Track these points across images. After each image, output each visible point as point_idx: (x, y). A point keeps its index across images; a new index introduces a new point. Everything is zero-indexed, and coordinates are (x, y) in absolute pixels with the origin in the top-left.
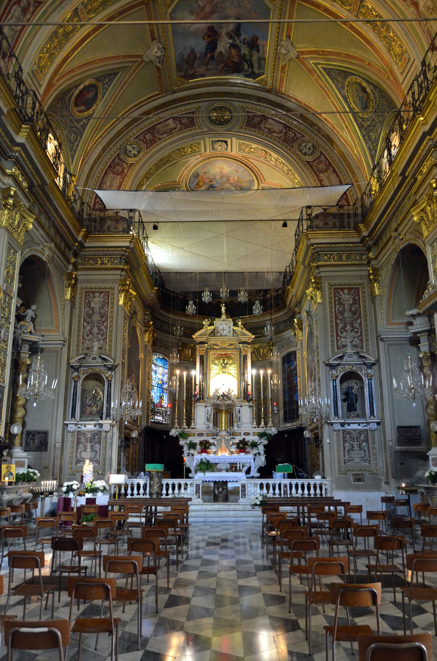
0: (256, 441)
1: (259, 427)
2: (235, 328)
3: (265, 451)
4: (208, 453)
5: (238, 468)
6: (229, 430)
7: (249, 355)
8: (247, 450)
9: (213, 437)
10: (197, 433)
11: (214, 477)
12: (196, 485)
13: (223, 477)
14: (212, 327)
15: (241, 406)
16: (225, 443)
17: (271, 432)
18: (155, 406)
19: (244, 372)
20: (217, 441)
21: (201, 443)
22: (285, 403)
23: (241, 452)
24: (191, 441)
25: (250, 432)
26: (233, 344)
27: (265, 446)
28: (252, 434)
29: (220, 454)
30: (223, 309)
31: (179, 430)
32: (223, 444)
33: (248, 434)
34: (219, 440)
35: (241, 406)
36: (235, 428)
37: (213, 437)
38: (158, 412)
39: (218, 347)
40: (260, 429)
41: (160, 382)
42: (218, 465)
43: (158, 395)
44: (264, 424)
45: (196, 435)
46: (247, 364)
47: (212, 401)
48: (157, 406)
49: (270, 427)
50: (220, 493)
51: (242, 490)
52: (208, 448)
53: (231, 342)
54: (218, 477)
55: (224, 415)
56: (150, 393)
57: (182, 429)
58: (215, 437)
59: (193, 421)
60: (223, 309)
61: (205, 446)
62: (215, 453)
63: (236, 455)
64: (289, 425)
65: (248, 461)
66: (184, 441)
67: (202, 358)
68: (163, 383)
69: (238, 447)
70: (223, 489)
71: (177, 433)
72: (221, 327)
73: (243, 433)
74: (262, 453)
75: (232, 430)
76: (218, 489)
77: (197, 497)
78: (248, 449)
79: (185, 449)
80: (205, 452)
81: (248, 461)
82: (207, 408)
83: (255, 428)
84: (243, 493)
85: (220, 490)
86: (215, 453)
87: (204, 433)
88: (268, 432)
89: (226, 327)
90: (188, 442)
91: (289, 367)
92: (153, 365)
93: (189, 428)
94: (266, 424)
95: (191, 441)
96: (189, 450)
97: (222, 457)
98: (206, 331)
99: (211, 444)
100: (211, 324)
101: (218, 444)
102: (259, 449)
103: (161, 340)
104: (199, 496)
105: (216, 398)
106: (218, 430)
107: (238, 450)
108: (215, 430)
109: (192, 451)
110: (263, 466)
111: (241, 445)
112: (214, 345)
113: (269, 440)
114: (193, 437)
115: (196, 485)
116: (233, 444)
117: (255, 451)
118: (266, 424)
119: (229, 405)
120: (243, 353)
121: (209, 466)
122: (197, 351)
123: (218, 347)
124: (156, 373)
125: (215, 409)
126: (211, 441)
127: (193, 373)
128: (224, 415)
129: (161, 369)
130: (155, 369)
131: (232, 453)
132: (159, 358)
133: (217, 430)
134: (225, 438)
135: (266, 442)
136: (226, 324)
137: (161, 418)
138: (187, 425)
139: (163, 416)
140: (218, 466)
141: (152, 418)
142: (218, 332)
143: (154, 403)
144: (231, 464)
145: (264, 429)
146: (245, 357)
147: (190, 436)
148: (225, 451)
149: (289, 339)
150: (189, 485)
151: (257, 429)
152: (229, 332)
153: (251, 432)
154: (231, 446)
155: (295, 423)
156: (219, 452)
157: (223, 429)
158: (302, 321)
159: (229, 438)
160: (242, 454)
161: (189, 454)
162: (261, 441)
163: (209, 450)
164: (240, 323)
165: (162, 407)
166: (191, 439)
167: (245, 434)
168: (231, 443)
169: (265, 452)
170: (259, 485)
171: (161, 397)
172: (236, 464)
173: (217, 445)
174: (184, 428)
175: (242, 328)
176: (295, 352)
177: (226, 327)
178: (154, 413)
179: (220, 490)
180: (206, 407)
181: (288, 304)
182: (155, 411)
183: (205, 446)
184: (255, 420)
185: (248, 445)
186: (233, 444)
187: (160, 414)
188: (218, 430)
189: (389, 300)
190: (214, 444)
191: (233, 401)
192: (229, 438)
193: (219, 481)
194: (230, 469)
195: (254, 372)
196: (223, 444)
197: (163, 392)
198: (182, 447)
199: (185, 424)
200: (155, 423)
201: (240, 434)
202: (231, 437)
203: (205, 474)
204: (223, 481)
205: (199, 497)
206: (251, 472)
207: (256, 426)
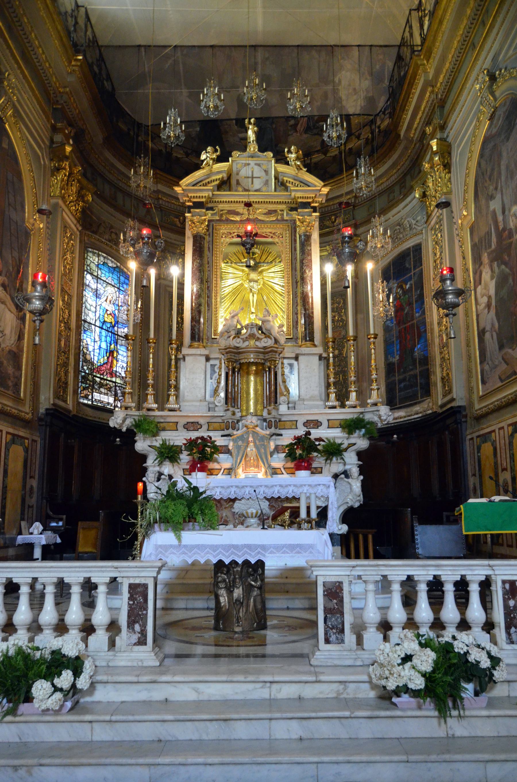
0: (338, 441)
1: (343, 406)
2: (282, 168)
3: (360, 466)
4: (211, 472)
5: (303, 514)
6: (265, 414)
7: (315, 236)
8: (314, 465)
9: (226, 432)
10: (182, 422)
11: (214, 548)
12: (132, 587)
13: (249, 547)
14: (223, 166)
15: (296, 358)
16: (256, 446)
17: (376, 419)
18: (94, 369)
19: (303, 273)
20: (234, 441)
21: (191, 444)
22: (390, 369)
23: (298, 468)
24: (164, 441)
25: (320, 418)
26: (275, 211)
27: (360, 454)
28: (325, 424)
29: (241, 474)
30: (251, 134)
31: (134, 412)
32: (251, 449)
33: (317, 424)
34: (241, 438)
35: (296, 358)
36: (283, 409)
37: (226, 432)
38: (101, 385)
39: (238, 218)
40: (346, 410)
41: (109, 319)
42: (237, 505)
43: (104, 345)
44: (358, 398)
45: (180, 426)
46: (310, 254)
47: (223, 343)
48: (99, 369)
49: (375, 404)
50: (239, 603)
51: (327, 611)
52: (210, 458)
53: (271, 207)
54: (228, 548)
55: (252, 378)
56: (79, 340)
57: (144, 412)
58: (230, 431)
59: (172, 392)
60: (251, 134)
61: (202, 451)
62: (230, 471)
63: (285, 478)
64: (401, 413)
65: (320, 491)
66: (148, 442)
67: (198, 240)
68: (117, 322)
69: (291, 455)
70: (248, 589)
71: (129, 422)
72: (245, 172)
73: (301, 420)
74: (355, 471)
75: (274, 413)
76: (230, 592)
77: (135, 638)
78: (319, 461)
79: (151, 462)
80: (202, 470)
81: (320, 493)
82: (212, 362)
83: (334, 407)
84: (333, 621)
85: (238, 593)
86: (230, 471)
87: (202, 421)
88: (368, 417)
89: (258, 172)
90: (158, 443)
91: (401, 287)
92: (88, 277)
93: (161, 408)
94: (362, 396)
95: (164, 441)
96: (160, 464)
97: (248, 483)
98: (209, 176)
99: (217, 450)
100: (223, 158)
101: (238, 448)
102: (347, 460)
103: (112, 227)
104: (143, 633)
105: (233, 333)
106: (238, 415)
107: (291, 465)
108: (229, 413)
109: (167, 469)
110: (357, 505)
111: (299, 452)
112: (231, 212)
113: (370, 438)
114: (174, 433)
115: (132, 587)
116: (277, 449)
117: (336, 467)
118: (362, 396)
119: (265, 351)
120: (301, 230)
121: (196, 508)
122: (188, 223)
123: (238, 218)
124: (97, 296)
125: (229, 360)
126: (220, 442)
127: (174, 271)
128: (252, 378)
129: (110, 290)
130: (94, 285)
131: (275, 472)
132: (104, 264)
133: (234, 414)
134: (255, 434)
135: (363, 444)
136: (259, 165)
137: (111, 400)
138: (156, 402)
139: (116, 395)
140: (238, 507)
141: (86, 397)
142: (238, 183)
143: (92, 364)
144: (271, 500)
145: (359, 409)
146: (307, 239)
147: (164, 429)
148: (257, 466)
149: (399, 225)
150: (102, 589)
151: (338, 410)
152: (267, 183)
153: (323, 419)
154: (272, 454)
155: (417, 408)
156: (240, 471)
157: (252, 410)
158: (449, 146)
159: (268, 432)
160: (303, 474)
161: (160, 474)
162: (352, 441)
163: (212, 465)
164: (293, 156)
165: (113, 374)
166: (165, 435)
167: (306, 424)
168: (272, 445)
169: (362, 470)
170: (396, 587)
171: (111, 352)
172: (298, 500)
173: (234, 453)
174: (149, 410)
175: (299, 168)
176: (418, 249)
177: (258, 172)
178: (93, 386)
179: (238, 593)
180: (208, 359)
181: (402, 134)
182: (94, 382)
183: (202, 451)
184: (332, 389)
185: (317, 451)
186: (277, 449)
187: (109, 389)
188: (238, 415)
189: (183, 584)
190: (227, 451)
191: (276, 341)
192: (268, 432)
193: (234, 563)
194: (274, 518)
195: (330, 268)
196: (251, 449)
197: (116, 343)
198: (144, 458)
199: (151, 398)
200: (92, 407)
201: (294, 424)
202: (273, 430)
203: (179, 538)
204: (247, 563)
205: (142, 642)
206: (329, 523)
207: (337, 403)
